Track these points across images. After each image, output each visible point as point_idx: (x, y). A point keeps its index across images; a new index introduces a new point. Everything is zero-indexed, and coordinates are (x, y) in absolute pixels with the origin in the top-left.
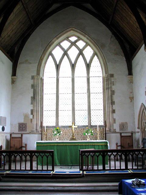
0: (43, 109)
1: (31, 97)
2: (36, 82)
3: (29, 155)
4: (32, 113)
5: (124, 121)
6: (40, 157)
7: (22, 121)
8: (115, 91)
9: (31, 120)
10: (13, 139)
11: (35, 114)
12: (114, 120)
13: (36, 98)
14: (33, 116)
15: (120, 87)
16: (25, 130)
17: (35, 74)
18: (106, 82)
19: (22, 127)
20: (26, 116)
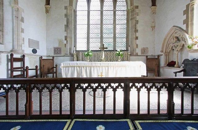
0: (76, 37)
1: (65, 25)
2: (69, 12)
3: (67, 86)
4: (66, 39)
5: (145, 47)
6: (99, 92)
7: (57, 46)
8: (139, 21)
9: (65, 45)
10: (44, 61)
11: (68, 40)
12: (137, 46)
13: (69, 26)
14: (67, 41)
15: (143, 18)
16: (60, 53)
17: (67, 4)
18: (131, 13)
19: (57, 51)
20: (60, 42)
